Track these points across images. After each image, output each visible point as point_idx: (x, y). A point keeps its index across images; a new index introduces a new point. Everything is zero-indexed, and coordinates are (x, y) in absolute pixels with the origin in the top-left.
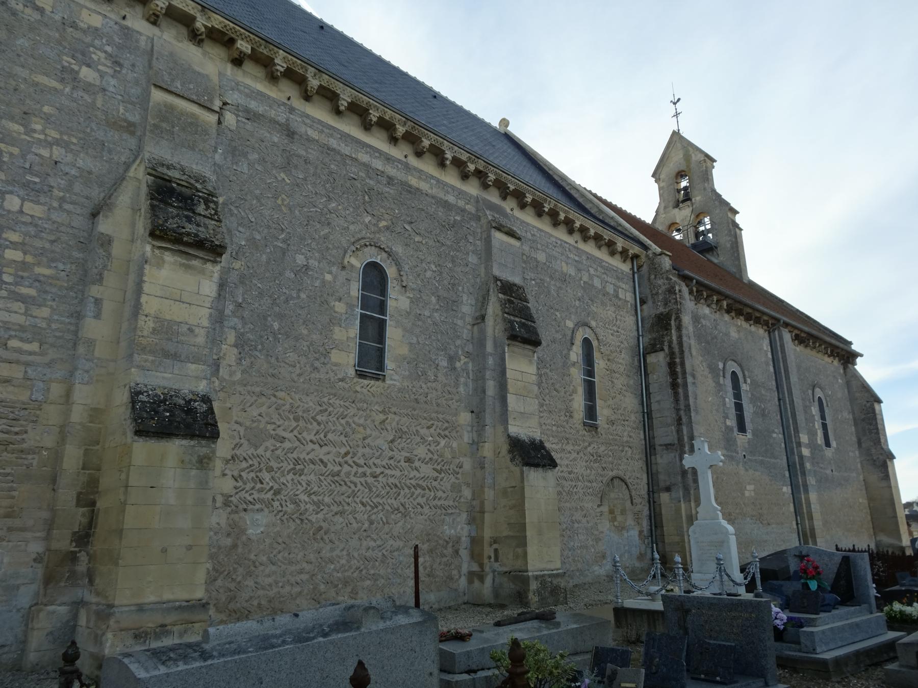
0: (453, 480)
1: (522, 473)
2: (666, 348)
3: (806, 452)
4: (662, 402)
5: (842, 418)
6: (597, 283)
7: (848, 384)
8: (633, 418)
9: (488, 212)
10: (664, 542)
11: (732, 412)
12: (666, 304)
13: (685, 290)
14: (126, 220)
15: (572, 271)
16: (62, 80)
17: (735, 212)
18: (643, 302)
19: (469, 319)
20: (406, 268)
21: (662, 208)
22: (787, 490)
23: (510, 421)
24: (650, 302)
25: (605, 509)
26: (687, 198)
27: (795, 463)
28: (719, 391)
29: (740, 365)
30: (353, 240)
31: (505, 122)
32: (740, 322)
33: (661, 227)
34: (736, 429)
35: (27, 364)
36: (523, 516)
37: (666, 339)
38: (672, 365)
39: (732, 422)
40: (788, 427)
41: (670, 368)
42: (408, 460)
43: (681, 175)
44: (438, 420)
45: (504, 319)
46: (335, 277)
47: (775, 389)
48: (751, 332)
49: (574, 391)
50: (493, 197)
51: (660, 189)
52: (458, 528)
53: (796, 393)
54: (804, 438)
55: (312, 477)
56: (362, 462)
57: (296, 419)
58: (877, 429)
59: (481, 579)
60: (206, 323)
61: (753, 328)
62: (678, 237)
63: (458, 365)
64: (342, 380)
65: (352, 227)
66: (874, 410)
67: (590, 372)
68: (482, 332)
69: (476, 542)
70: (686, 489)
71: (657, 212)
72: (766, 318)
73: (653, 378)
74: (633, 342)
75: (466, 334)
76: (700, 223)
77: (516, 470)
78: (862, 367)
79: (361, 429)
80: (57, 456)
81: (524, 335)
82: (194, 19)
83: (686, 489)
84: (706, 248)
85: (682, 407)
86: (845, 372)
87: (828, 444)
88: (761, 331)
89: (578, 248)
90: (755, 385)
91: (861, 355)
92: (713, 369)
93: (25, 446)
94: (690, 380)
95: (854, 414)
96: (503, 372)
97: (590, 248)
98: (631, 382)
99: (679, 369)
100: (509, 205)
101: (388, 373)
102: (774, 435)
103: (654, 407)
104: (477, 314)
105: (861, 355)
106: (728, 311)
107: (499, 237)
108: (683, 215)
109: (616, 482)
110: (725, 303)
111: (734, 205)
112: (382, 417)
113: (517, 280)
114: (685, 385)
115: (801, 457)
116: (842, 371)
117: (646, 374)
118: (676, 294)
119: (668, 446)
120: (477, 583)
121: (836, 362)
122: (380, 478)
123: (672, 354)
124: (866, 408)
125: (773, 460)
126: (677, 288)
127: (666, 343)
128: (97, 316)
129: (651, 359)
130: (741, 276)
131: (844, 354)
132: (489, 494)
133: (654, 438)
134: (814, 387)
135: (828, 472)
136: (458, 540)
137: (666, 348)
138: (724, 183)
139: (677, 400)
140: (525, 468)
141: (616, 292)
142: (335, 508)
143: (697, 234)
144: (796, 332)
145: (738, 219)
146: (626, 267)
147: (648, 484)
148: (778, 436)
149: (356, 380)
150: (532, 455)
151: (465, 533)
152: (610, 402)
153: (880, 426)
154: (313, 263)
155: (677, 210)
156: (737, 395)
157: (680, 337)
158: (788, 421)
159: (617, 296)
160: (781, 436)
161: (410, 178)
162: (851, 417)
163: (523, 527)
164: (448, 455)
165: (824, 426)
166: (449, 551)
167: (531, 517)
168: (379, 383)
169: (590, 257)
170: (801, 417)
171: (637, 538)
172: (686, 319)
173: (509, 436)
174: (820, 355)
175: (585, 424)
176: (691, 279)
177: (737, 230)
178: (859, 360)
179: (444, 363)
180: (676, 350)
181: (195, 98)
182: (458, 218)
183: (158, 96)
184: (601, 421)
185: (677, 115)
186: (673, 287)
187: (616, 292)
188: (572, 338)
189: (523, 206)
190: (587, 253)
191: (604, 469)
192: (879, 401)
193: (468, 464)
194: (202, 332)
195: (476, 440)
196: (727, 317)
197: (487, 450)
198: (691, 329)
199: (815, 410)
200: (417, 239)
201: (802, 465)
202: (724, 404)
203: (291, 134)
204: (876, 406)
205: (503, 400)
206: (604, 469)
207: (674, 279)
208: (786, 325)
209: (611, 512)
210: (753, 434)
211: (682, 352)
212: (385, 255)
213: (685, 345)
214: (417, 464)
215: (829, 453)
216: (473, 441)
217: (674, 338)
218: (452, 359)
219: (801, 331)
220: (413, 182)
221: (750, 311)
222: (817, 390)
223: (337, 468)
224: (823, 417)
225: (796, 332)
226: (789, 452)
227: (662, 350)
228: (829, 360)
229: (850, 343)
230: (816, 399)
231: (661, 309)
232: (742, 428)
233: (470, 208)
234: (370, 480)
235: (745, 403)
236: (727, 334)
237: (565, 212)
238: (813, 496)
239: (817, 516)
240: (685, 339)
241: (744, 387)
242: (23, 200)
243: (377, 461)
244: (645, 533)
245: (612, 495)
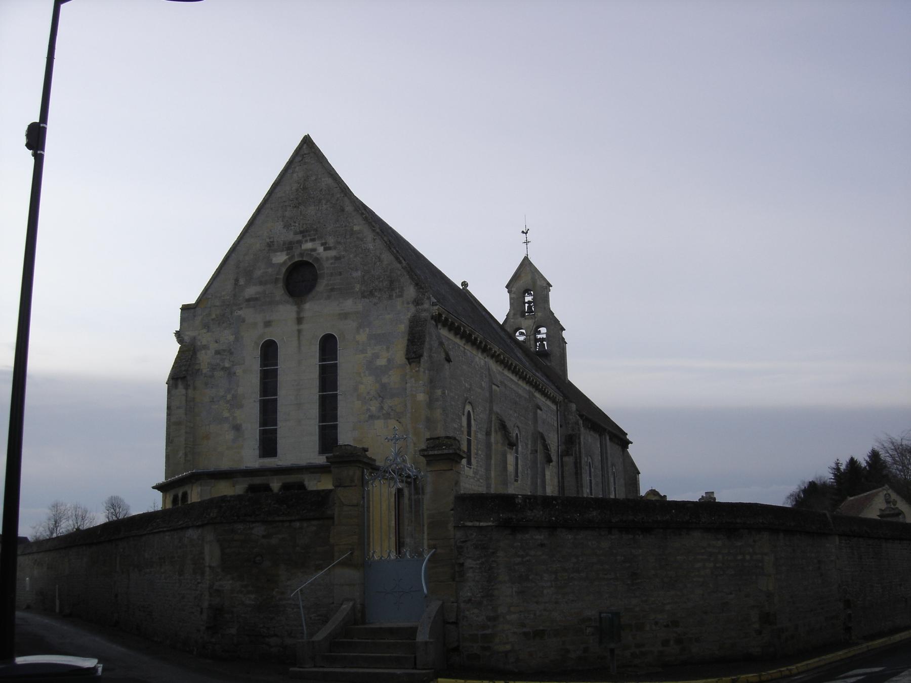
17: (563, 329)
31: (465, 284)
32: (592, 433)
38: (576, 463)
43: (527, 291)
51: (511, 299)
78: (631, 449)
84: (544, 354)
107: (539, 411)
117: (562, 466)
129: (566, 459)
131: (621, 439)
138: (558, 304)
145: (564, 334)
146: (554, 407)
157: (580, 449)
185: (527, 242)
192: (639, 473)
231: (570, 432)
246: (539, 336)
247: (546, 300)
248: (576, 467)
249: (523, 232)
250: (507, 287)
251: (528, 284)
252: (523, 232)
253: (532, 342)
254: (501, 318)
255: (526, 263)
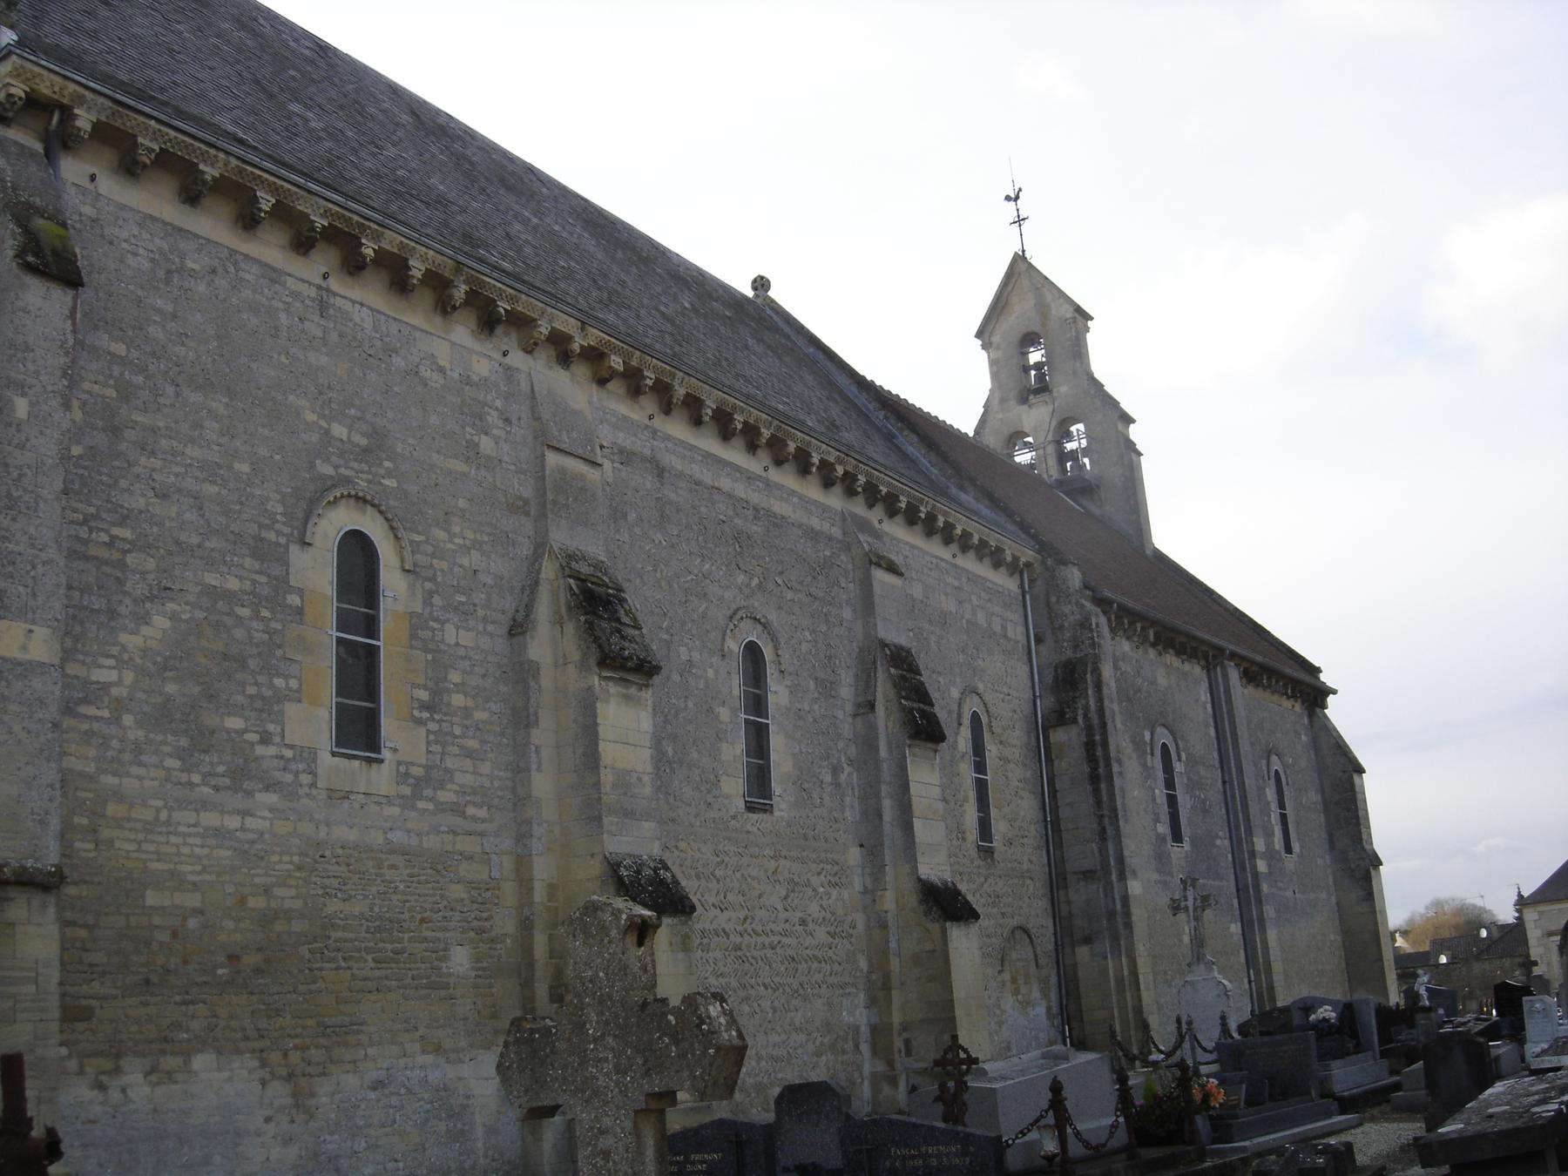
0: (848, 946)
1: (944, 932)
2: (1080, 720)
3: (1262, 866)
4: (1076, 804)
5: (1306, 800)
6: (981, 618)
7: (1315, 743)
8: (1032, 828)
9: (862, 538)
10: (1081, 1021)
11: (1164, 809)
12: (1076, 647)
13: (1103, 620)
14: (552, 643)
15: (952, 606)
16: (467, 460)
17: (1128, 420)
18: (1039, 640)
19: (849, 708)
20: (782, 641)
21: (996, 401)
22: (1235, 928)
23: (920, 859)
24: (1050, 642)
25: (1007, 976)
26: (1043, 388)
27: (1247, 886)
28: (1147, 778)
29: (1173, 733)
30: (729, 613)
31: (761, 284)
32: (1170, 659)
33: (993, 442)
34: (1169, 838)
35: (482, 834)
36: (948, 988)
37: (1080, 703)
38: (1089, 746)
39: (1164, 828)
40: (1237, 828)
41: (1087, 751)
42: (803, 922)
43: (1030, 340)
44: (827, 862)
45: (903, 708)
46: (717, 672)
47: (1217, 763)
48: (1184, 673)
49: (966, 800)
50: (858, 507)
52: (856, 1013)
53: (1248, 768)
54: (1260, 844)
55: (718, 954)
56: (759, 929)
57: (698, 878)
58: (1357, 817)
59: (893, 1081)
60: (650, 769)
61: (1187, 667)
62: (1023, 458)
63: (843, 777)
64: (734, 817)
65: (727, 594)
66: (1352, 785)
67: (980, 767)
68: (872, 727)
69: (879, 1032)
70: (1115, 938)
71: (986, 406)
72: (1204, 648)
73: (1059, 766)
74: (1028, 708)
75: (846, 730)
76: (1068, 436)
77: (935, 927)
78: (1335, 710)
79: (755, 884)
80: (526, 948)
81: (927, 731)
82: (570, 338)
83: (1115, 938)
84: (1082, 488)
85: (1106, 812)
86: (1311, 722)
87: (1289, 850)
88: (1197, 670)
89: (955, 566)
90: (1192, 762)
91: (1334, 692)
92: (1138, 744)
93: (493, 934)
94: (1115, 768)
95: (1323, 793)
96: (904, 787)
97: (969, 562)
98: (1029, 774)
99: (1099, 753)
100: (875, 515)
101: (776, 800)
102: (1218, 842)
103: (1064, 812)
104: (861, 699)
105: (1334, 692)
106: (1154, 645)
107: (880, 575)
108: (1036, 417)
109: (1018, 934)
110: (1151, 632)
111: (1126, 406)
112: (773, 864)
113: (902, 640)
114: (1110, 777)
115: (1256, 875)
116: (1306, 721)
117: (1049, 759)
118: (1091, 630)
119: (1088, 875)
120: (887, 1090)
121: (1298, 707)
122: (778, 950)
123: (1089, 729)
124: (1339, 775)
125: (1217, 883)
126: (1094, 621)
127: (1080, 712)
128: (539, 770)
129: (1059, 736)
130: (1143, 545)
131: (1302, 686)
132: (895, 964)
133: (1063, 861)
134: (1269, 753)
135: (1289, 894)
136: (857, 1030)
137: (1080, 720)
138: (1110, 359)
139: (1099, 803)
140: (948, 924)
141: (1004, 628)
142: (742, 994)
143: (1063, 457)
144: (1245, 664)
145: (1134, 433)
146: (1011, 584)
147: (1055, 934)
148: (1223, 843)
149: (746, 815)
150: (946, 904)
151: (865, 1021)
152: (1006, 810)
153: (1361, 813)
154: (696, 655)
155: (1025, 407)
156: (1170, 784)
157: (1100, 700)
158: (1236, 817)
159: (1005, 636)
160: (1227, 842)
161: (772, 501)
162: (1319, 797)
163: (950, 1005)
164: (840, 912)
165: (1283, 818)
166: (849, 1046)
167: (959, 993)
168: (765, 816)
169: (973, 578)
170: (1254, 809)
171: (1044, 1018)
172: (1107, 671)
173: (919, 879)
174: (1275, 697)
175: (979, 847)
176: (1110, 602)
177: (1134, 456)
178: (1331, 699)
179: (828, 778)
180: (1095, 721)
181: (580, 452)
182: (827, 553)
183: (552, 459)
184: (997, 843)
185: (1019, 221)
186: (1088, 619)
187: (1004, 628)
188: (960, 716)
189: (892, 513)
190: (967, 571)
191: (1003, 914)
192: (1361, 770)
193: (860, 920)
194: (646, 779)
195: (870, 887)
196: (1152, 653)
197: (889, 902)
198: (1113, 684)
199: (1271, 794)
200: (790, 595)
201: (1257, 887)
202: (1154, 800)
203: (660, 472)
204: (1355, 777)
205: (908, 828)
206: (1003, 914)
207: (1088, 605)
208: (1233, 655)
209: (1014, 980)
210: (1193, 844)
211: (1104, 725)
212: (760, 628)
213: (1107, 712)
214: (811, 926)
215: (1290, 862)
216: (865, 888)
217: (1092, 702)
218: (836, 770)
219: (1253, 662)
220: (779, 507)
221: (1183, 639)
222: (1274, 758)
223: (739, 940)
224: (1282, 805)
225: (1245, 664)
226: (1239, 867)
227: (1075, 721)
228: (1287, 703)
229: (1318, 670)
230: (1272, 774)
231: (1069, 654)
232: (1177, 837)
233: (836, 532)
234: (770, 953)
235: (1180, 793)
236: (1154, 683)
237: (945, 514)
238: (1272, 935)
239: (1277, 967)
240: (1106, 703)
241: (1178, 767)
242: (457, 628)
243: (773, 927)
244: (1055, 1010)
245: (1014, 955)
246: (1070, 446)
247: (1079, 351)
248: (1091, 759)
249: (1008, 198)
250: (979, 335)
251: (1033, 325)
252: (1008, 198)
253: (1052, 462)
254: (964, 419)
255: (1020, 271)
